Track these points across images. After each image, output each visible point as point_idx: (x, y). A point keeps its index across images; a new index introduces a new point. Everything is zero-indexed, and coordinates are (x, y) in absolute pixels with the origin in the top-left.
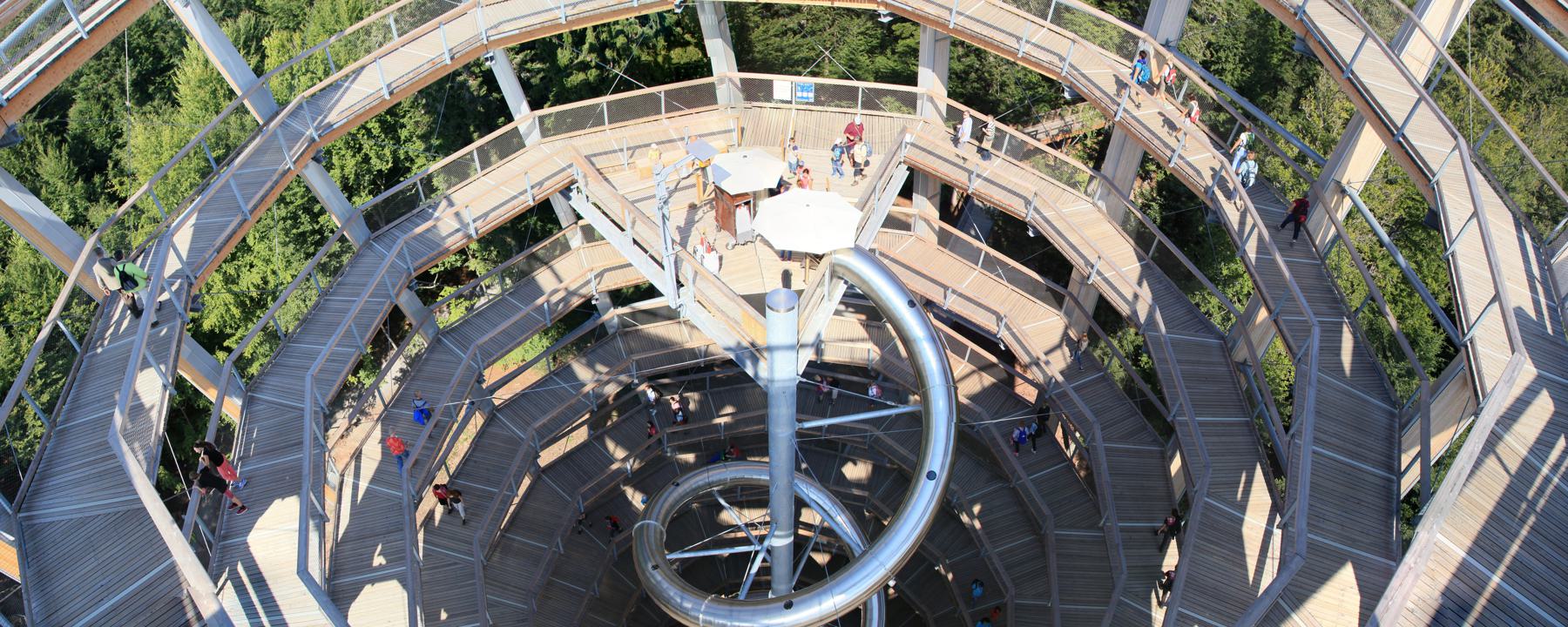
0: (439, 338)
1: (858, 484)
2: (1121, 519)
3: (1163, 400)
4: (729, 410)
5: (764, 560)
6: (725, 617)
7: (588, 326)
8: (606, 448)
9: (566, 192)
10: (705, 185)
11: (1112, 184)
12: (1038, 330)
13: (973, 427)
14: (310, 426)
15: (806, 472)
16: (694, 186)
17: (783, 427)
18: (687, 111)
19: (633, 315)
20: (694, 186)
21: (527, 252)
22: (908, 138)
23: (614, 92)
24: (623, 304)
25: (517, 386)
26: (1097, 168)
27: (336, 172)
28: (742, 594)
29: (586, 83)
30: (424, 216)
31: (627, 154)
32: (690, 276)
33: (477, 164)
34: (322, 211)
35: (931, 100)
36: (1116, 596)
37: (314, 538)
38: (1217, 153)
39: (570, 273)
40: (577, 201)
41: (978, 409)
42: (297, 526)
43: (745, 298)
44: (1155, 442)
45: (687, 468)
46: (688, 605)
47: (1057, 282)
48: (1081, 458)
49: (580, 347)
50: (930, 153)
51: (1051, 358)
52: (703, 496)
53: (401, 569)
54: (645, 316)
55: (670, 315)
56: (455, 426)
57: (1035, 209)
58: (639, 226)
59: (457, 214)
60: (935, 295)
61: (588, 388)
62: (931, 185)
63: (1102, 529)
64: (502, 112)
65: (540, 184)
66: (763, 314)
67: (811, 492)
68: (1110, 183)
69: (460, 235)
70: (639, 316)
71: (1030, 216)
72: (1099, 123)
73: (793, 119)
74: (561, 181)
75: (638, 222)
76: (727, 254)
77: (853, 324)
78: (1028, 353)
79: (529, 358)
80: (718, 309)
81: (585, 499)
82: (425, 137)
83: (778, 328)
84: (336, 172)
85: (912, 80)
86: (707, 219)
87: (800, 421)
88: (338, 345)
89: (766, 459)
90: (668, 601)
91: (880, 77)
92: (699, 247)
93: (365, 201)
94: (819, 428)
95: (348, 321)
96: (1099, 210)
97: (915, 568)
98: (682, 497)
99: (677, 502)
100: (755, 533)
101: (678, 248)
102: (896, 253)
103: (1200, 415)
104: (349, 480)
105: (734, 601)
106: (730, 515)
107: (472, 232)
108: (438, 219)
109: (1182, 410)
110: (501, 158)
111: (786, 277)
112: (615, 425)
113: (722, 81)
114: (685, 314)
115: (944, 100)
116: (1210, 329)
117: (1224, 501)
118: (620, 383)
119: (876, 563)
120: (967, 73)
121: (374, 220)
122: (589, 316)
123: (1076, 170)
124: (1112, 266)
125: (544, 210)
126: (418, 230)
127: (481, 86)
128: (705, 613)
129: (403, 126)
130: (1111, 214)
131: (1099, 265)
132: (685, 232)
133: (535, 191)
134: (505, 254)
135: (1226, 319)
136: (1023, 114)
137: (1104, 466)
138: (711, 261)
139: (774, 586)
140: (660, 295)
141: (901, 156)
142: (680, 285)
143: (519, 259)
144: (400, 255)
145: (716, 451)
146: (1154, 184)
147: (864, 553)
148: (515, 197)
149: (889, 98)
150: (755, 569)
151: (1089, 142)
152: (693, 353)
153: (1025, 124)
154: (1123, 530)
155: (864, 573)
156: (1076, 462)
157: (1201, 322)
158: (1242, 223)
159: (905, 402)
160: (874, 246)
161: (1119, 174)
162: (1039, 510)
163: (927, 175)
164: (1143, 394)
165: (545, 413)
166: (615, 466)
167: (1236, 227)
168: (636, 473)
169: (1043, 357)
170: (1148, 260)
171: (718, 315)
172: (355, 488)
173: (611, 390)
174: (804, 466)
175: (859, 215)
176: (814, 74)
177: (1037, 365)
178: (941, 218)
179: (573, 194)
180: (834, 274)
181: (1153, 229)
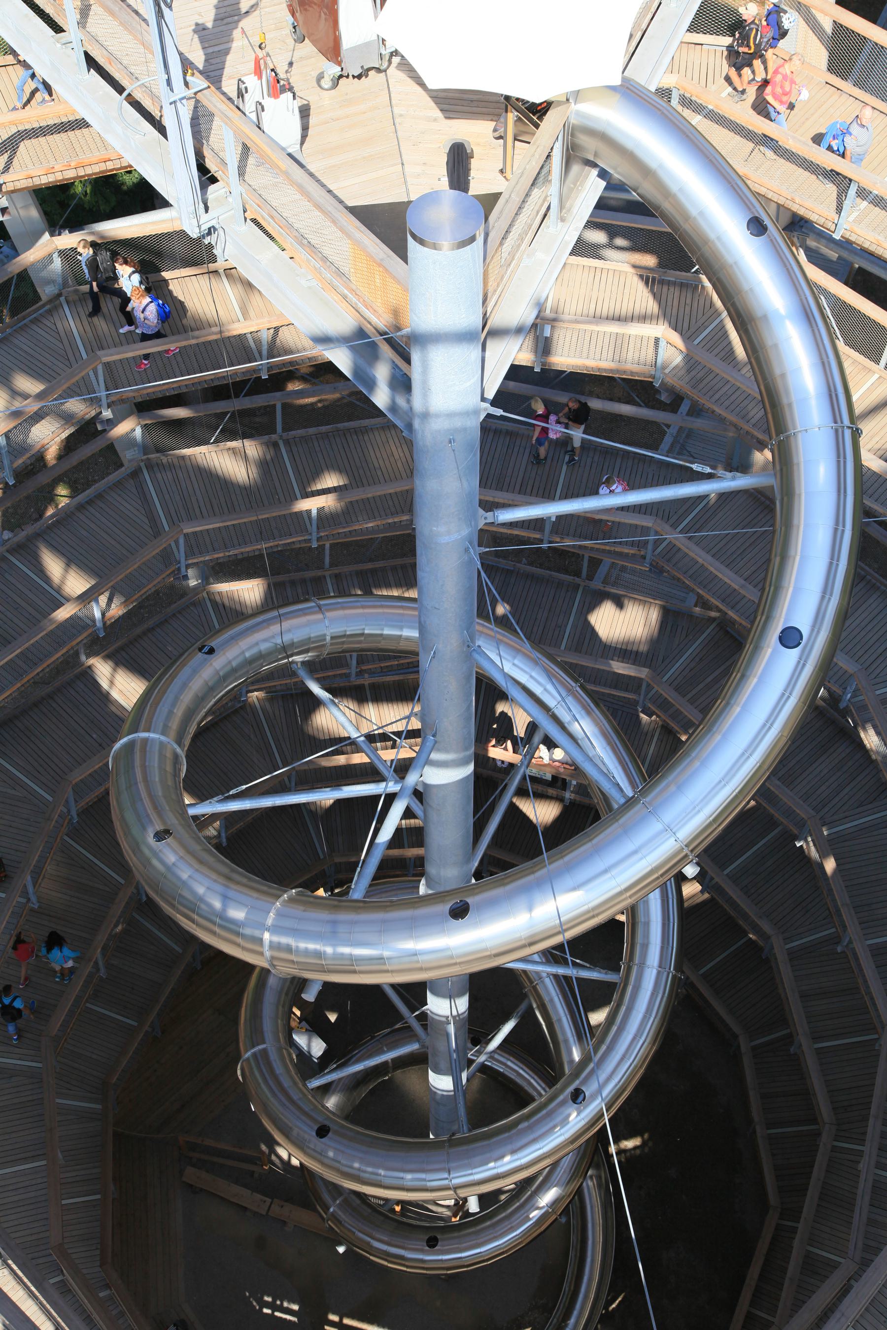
1: (624, 651)
5: (408, 814)
8: (47, 579)
15: (502, 622)
17: (449, 524)
24: (74, 225)
28: (359, 887)
32: (232, 158)
43: (356, 212)
45: (233, 615)
46: (238, 914)
52: (271, 675)
55: (197, 253)
60: (814, 201)
66: (402, 253)
76: (323, 103)
77: (621, 277)
80: (302, 240)
83: (438, 288)
87: (488, 506)
89: (413, 594)
90: (193, 907)
92: (251, 81)
94: (537, 524)
97: (746, 841)
99: (210, 690)
100: (388, 755)
101: (198, 82)
111: (459, 161)
112: (65, 518)
114: (226, 252)
118: (67, 418)
119: (559, 1169)
128: (275, 929)
132: (215, 39)
139: (431, 869)
140: (165, 204)
142: (207, 177)
145: (301, 572)
147: (630, 803)
150: (386, 833)
152: (241, 348)
155: (629, 846)
160: (669, 81)
166: (63, 614)
168: (114, 628)
171: (302, 254)
173: (48, 436)
174: (501, 609)
180: (573, 155)
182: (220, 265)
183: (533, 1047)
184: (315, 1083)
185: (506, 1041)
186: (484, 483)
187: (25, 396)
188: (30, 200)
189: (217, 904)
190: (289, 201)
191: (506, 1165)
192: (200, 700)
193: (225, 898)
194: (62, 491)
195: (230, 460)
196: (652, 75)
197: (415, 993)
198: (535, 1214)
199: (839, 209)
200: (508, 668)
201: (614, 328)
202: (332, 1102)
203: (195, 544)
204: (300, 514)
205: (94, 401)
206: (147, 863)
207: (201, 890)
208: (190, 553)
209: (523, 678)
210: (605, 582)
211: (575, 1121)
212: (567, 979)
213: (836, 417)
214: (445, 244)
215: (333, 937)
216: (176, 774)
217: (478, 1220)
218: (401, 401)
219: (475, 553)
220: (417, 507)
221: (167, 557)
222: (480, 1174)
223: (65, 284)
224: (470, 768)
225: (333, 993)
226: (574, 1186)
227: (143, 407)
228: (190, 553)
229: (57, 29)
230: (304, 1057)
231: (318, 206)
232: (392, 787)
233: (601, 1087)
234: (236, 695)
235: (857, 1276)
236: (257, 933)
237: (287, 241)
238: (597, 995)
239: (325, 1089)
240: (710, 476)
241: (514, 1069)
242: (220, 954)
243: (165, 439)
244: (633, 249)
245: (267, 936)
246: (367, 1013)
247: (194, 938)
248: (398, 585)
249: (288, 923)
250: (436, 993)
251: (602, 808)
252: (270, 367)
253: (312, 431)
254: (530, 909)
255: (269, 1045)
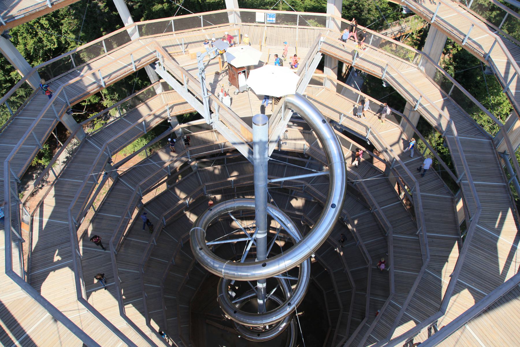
0: (86, 140)
1: (298, 209)
2: (381, 207)
3: (454, 172)
4: (235, 173)
5: (253, 244)
6: (234, 270)
7: (166, 133)
9: (153, 65)
10: (223, 63)
11: (428, 57)
12: (387, 134)
13: (353, 183)
14: (8, 191)
16: (218, 63)
17: (261, 182)
18: (214, 26)
19: (188, 128)
20: (218, 63)
21: (133, 95)
22: (322, 39)
23: (178, 15)
24: (184, 123)
25: (131, 164)
26: (419, 49)
27: (21, 47)
28: (243, 260)
29: (162, 10)
30: (76, 75)
31: (184, 46)
32: (216, 108)
33: (105, 48)
34: (13, 69)
35: (333, 20)
36: (423, 268)
37: (15, 252)
38: (493, 34)
39: (155, 107)
40: (159, 70)
41: (356, 174)
42: (4, 247)
43: (241, 118)
44: (448, 193)
46: (217, 266)
47: (397, 109)
48: (407, 200)
49: (164, 144)
50: (333, 46)
51: (393, 148)
52: (224, 215)
53: (70, 260)
54: (195, 128)
55: (208, 127)
56: (97, 186)
57: (387, 73)
58: (191, 83)
59: (94, 74)
60: (335, 117)
61: (166, 165)
62: (333, 62)
63: (418, 236)
64: (119, 22)
65: (139, 60)
66: (251, 127)
67: (275, 212)
68: (427, 57)
69: (95, 85)
70: (192, 128)
71: (384, 76)
72: (420, 26)
73: (266, 31)
74: (150, 59)
75: (190, 81)
76: (235, 97)
77: (296, 131)
78: (382, 146)
79: (136, 149)
80: (230, 124)
81: (166, 218)
82: (74, 32)
84: (21, 47)
85: (324, 10)
86: (225, 80)
87: (270, 179)
88: (24, 144)
89: (254, 197)
90: (207, 264)
91: (306, 10)
92: (221, 94)
93: (38, 64)
94: (280, 182)
95: (30, 131)
96: (421, 71)
97: (324, 249)
98: (214, 216)
99: (211, 218)
101: (210, 94)
102: (316, 96)
103: (476, 180)
104: (37, 218)
105: (239, 263)
106: (237, 224)
107: (103, 84)
108: (83, 76)
109: (465, 176)
110: (118, 46)
111: (263, 109)
112: (180, 182)
113: (231, 13)
114: (215, 127)
115: (339, 20)
116: (483, 134)
117: (487, 227)
118: (182, 161)
119: (305, 247)
120: (350, 6)
121: (44, 74)
122: (167, 128)
123: (408, 51)
124: (428, 101)
125: (142, 74)
126: (72, 82)
127: (105, 7)
128: (225, 269)
129: (62, 24)
130: (428, 73)
131: (421, 101)
132: (213, 86)
133: (137, 64)
134: (122, 96)
135: (492, 129)
136: (378, 25)
137: (420, 204)
138: (226, 101)
139: (258, 256)
140: (203, 118)
141: (318, 48)
142: (211, 112)
143: (128, 99)
144: (61, 95)
145: (229, 193)
146: (451, 56)
147: (300, 241)
148: (125, 67)
149: (311, 20)
150: (248, 249)
151: (414, 36)
152: (218, 146)
153: (380, 30)
154: (429, 237)
155: (300, 251)
156: (404, 202)
157: (478, 130)
158: (507, 72)
159: (321, 170)
160: (305, 93)
161: (432, 52)
162: (385, 224)
163: (331, 57)
164: (443, 168)
165: (145, 177)
166: (180, 202)
167: (503, 75)
168: (191, 205)
169: (389, 148)
170: (448, 97)
171: (231, 127)
172: (41, 222)
174: (272, 200)
175: (299, 78)
176: (274, 9)
177: (386, 152)
178: (338, 79)
179: (157, 66)
180: (286, 107)
181: (451, 80)
182: (214, 129)
183: (280, 294)
184: (234, 302)
185: (274, 293)
186: (269, 174)
187: (173, 157)
188: (175, 118)
189: (212, 263)
190: (228, 117)
191: (275, 319)
192: (209, 220)
193: (214, 262)
194: (180, 176)
195: (217, 170)
196: (302, 93)
197: (255, 283)
198: (280, 329)
199: (340, 119)
200: (274, 213)
201: (294, 142)
202: (237, 306)
203: (208, 187)
204: (230, 181)
205: (188, 158)
206: (198, 255)
207: (209, 261)
208: (207, 189)
209: (277, 215)
210: (294, 195)
211: (289, 309)
212: (287, 279)
213: (341, 160)
214: (260, 125)
215: (236, 270)
216: (204, 236)
217: (268, 330)
218: (251, 156)
219: (267, 189)
220: (255, 179)
221: (202, 190)
222: (269, 321)
223: (182, 134)
224: (266, 234)
225: (237, 283)
226: (288, 323)
227: (197, 159)
228: (207, 189)
229: (182, 85)
230: (231, 296)
231: (234, 118)
232: (250, 239)
233: (295, 302)
234: (216, 219)
235: (347, 339)
236: (221, 269)
237: (228, 125)
238: (293, 282)
239: (236, 303)
240: (316, 172)
241: (276, 299)
242: (213, 274)
243: (202, 165)
244: (298, 126)
245: (223, 270)
246: (245, 287)
247: (207, 271)
248: (250, 195)
249: (227, 268)
250: (259, 283)
251: (294, 243)
252: (224, 150)
253: (232, 163)
254: (279, 265)
255: (224, 294)
